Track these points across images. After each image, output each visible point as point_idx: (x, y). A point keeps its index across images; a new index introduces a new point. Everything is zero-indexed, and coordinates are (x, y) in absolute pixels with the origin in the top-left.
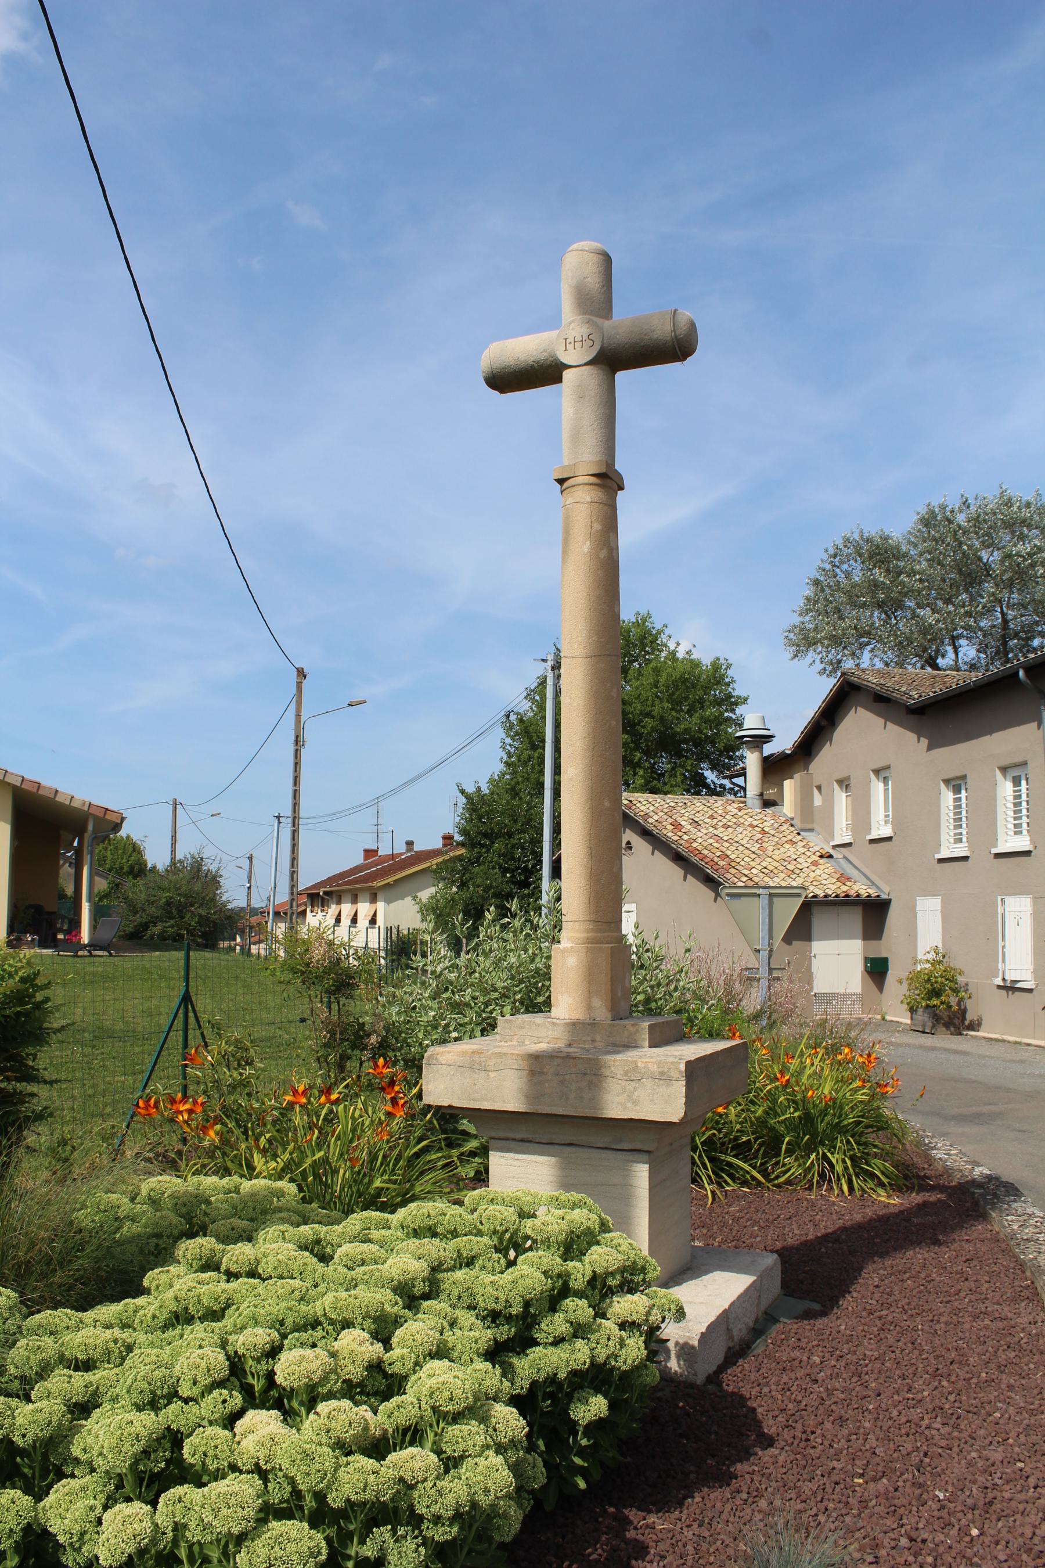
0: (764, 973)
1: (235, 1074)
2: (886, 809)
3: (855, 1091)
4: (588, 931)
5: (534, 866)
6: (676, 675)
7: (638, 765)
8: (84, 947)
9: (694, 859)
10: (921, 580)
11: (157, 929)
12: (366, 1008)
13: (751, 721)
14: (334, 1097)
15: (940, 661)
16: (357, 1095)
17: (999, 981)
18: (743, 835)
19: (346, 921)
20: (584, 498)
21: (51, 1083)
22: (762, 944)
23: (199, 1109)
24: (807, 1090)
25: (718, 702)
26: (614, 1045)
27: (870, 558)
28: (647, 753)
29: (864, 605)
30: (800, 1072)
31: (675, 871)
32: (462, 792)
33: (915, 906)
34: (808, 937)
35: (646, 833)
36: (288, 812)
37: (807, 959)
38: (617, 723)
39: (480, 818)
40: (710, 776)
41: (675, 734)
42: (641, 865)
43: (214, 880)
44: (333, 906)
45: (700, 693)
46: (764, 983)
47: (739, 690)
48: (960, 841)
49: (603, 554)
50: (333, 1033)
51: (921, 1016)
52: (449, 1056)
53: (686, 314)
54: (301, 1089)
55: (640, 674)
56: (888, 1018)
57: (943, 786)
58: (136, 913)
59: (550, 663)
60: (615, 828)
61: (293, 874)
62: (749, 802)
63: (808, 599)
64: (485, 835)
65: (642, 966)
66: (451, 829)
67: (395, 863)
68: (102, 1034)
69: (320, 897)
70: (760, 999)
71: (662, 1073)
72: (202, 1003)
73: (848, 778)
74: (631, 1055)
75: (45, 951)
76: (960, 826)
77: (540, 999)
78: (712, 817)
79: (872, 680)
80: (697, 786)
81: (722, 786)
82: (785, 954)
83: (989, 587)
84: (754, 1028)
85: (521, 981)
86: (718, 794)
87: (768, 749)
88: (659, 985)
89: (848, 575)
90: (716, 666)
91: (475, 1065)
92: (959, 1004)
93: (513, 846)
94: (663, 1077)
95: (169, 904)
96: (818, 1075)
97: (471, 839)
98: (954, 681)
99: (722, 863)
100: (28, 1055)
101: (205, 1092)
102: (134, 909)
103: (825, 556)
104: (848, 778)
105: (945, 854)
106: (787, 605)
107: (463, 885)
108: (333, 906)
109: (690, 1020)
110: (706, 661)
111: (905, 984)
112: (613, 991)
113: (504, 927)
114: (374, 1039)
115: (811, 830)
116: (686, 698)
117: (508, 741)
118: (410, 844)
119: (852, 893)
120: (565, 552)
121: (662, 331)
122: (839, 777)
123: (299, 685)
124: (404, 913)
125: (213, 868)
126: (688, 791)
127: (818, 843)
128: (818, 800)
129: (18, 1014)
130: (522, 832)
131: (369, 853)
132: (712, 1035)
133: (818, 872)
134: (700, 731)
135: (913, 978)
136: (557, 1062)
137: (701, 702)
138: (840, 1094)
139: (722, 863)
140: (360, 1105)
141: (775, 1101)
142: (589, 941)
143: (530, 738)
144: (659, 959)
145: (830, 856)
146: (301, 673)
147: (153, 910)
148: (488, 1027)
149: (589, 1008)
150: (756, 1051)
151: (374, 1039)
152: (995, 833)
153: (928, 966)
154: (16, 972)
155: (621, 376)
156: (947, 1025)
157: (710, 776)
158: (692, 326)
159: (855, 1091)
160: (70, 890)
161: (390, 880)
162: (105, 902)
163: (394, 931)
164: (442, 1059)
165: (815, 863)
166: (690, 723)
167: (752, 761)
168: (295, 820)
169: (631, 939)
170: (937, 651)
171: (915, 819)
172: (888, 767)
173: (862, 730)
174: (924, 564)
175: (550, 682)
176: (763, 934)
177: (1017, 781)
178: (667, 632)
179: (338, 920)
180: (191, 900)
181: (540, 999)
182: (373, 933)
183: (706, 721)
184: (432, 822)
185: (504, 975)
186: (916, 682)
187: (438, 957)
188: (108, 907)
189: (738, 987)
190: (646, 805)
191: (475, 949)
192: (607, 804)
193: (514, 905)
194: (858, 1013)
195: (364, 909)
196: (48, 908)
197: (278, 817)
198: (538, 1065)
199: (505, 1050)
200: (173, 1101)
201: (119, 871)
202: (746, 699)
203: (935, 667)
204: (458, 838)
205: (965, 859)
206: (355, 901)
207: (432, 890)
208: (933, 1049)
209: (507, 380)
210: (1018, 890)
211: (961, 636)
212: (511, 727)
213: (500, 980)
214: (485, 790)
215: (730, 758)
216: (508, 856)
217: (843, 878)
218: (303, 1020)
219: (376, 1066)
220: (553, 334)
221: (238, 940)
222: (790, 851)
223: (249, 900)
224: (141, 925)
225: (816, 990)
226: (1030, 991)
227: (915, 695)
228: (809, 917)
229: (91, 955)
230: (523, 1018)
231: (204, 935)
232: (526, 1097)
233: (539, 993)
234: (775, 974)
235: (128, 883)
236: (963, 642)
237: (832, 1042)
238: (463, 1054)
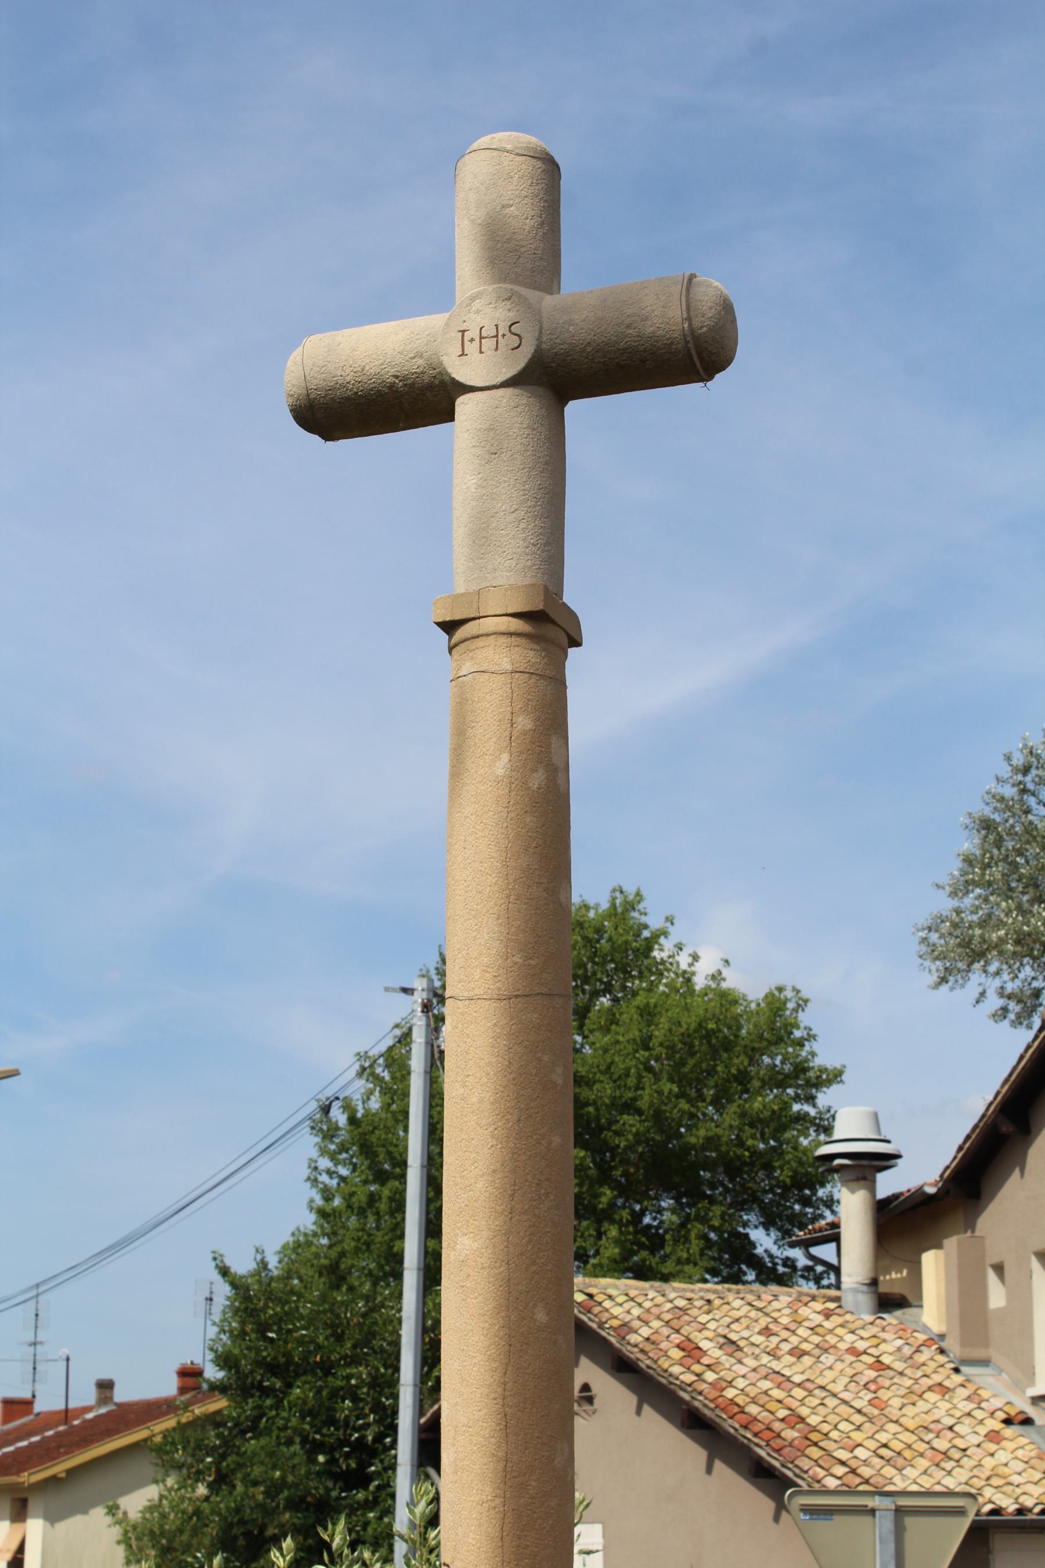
5: (379, 1438)
6: (689, 1022)
7: (606, 1215)
9: (731, 1425)
18: (835, 1372)
20: (497, 661)
25: (778, 1080)
28: (627, 1191)
31: (687, 1452)
32: (224, 1272)
35: (623, 1367)
39: (262, 1330)
40: (764, 1241)
41: (687, 1148)
42: (616, 1441)
45: (740, 1061)
47: (824, 1055)
49: (538, 779)
53: (714, 283)
59: (419, 997)
60: (559, 1359)
62: (848, 1299)
63: (969, 861)
64: (273, 1368)
67: (72, 1432)
80: (734, 1262)
86: (782, 1281)
93: (334, 1394)
97: (241, 1376)
99: (790, 1434)
106: (926, 874)
107: (221, 1481)
110: (750, 985)
115: (985, 1362)
116: (711, 1072)
117: (325, 1163)
118: (105, 1387)
121: (664, 318)
126: (714, 1272)
127: (1000, 1392)
128: (997, 1296)
130: (354, 1361)
133: (1002, 1456)
137: (743, 1078)
139: (790, 1434)
143: (374, 1154)
145: (1027, 1421)
155: (576, 410)
157: (764, 1241)
158: (727, 309)
161: (59, 1468)
165: (994, 1436)
166: (715, 1124)
167: (852, 1209)
178: (676, 934)
183: (754, 1122)
190: (622, 1303)
192: (541, 1316)
204: (213, 1373)
207: (151, 1492)
209: (338, 414)
216: (322, 1414)
220: (436, 321)
222: (940, 1408)
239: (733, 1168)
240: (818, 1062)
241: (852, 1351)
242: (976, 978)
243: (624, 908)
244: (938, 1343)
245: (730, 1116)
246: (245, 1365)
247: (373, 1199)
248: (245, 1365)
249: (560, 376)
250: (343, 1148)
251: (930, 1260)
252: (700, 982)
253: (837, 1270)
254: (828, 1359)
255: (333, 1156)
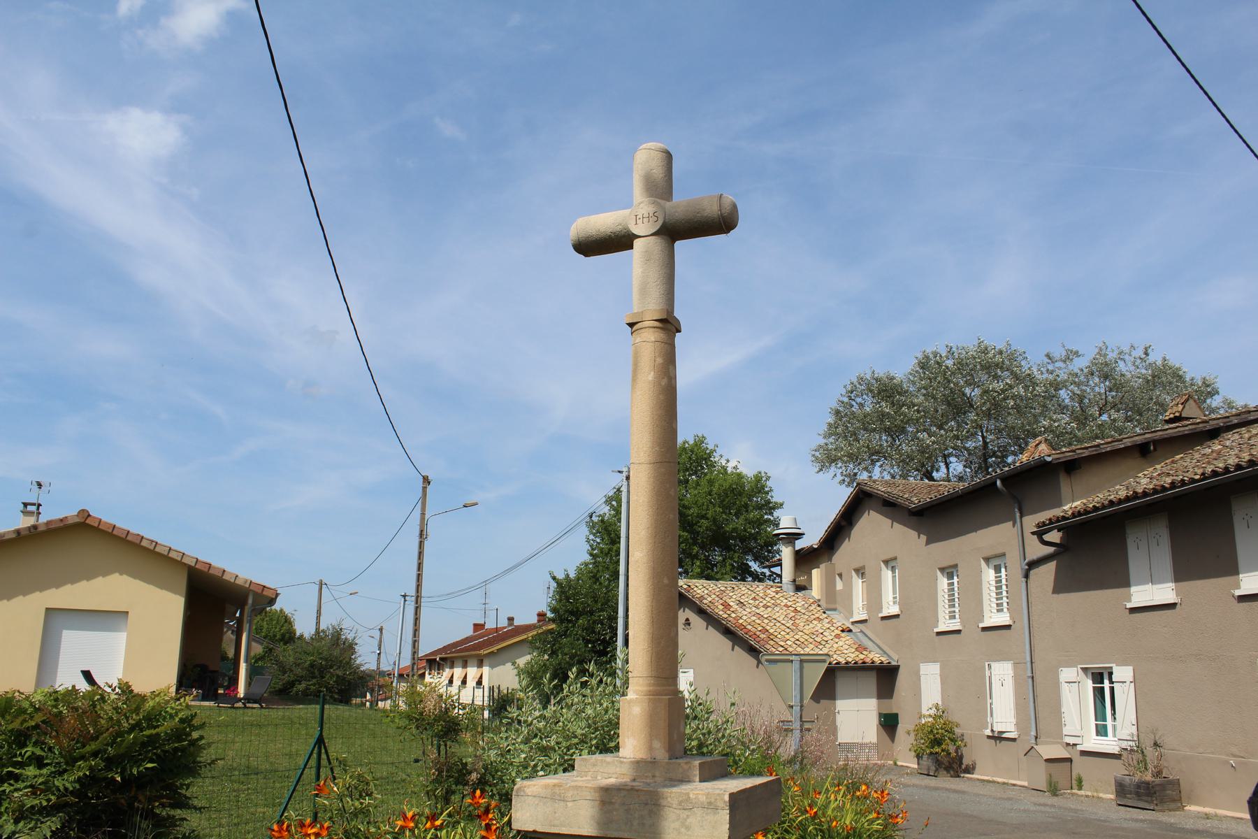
0: (797, 725)
1: (357, 803)
2: (894, 592)
3: (871, 822)
4: (649, 685)
5: (611, 638)
6: (726, 485)
7: (696, 557)
8: (240, 700)
9: (741, 633)
10: (918, 411)
11: (302, 687)
12: (468, 750)
13: (786, 522)
14: (438, 823)
15: (935, 474)
16: (459, 823)
17: (988, 732)
18: (780, 614)
19: (457, 682)
20: (649, 338)
21: (200, 809)
22: (795, 701)
23: (324, 833)
24: (831, 821)
25: (759, 507)
26: (671, 780)
27: (879, 393)
28: (703, 547)
29: (874, 430)
30: (826, 806)
31: (726, 643)
32: (554, 578)
33: (919, 671)
34: (832, 696)
35: (701, 612)
36: (412, 592)
37: (833, 714)
38: (675, 517)
39: (568, 599)
40: (754, 566)
41: (725, 532)
42: (695, 639)
43: (350, 647)
44: (447, 670)
45: (745, 499)
46: (797, 733)
47: (776, 497)
48: (954, 617)
49: (664, 382)
50: (440, 771)
51: (926, 761)
52: (534, 789)
53: (729, 197)
54: (409, 815)
55: (698, 484)
56: (899, 763)
57: (939, 573)
58: (285, 673)
59: (625, 474)
60: (673, 605)
61: (415, 643)
62: (785, 587)
63: (830, 425)
64: (572, 613)
65: (695, 718)
66: (544, 608)
67: (499, 635)
68: (250, 772)
69: (436, 662)
70: (793, 748)
71: (710, 803)
72: (336, 748)
73: (863, 567)
74: (685, 788)
75: (206, 703)
76: (954, 606)
77: (612, 744)
78: (754, 599)
79: (881, 489)
80: (743, 573)
81: (763, 574)
82: (814, 710)
83: (972, 416)
84: (788, 771)
85: (596, 729)
86: (761, 580)
87: (800, 544)
88: (709, 732)
89: (861, 405)
90: (758, 478)
91: (555, 796)
92: (956, 752)
93: (594, 622)
94: (711, 807)
95: (312, 665)
96: (840, 809)
97: (560, 616)
98: (946, 489)
99: (762, 636)
100: (182, 785)
101: (331, 818)
102: (283, 669)
103: (844, 392)
104: (863, 567)
105: (942, 628)
106: (814, 429)
107: (553, 653)
108: (447, 670)
109: (735, 762)
110: (748, 471)
111: (913, 735)
112: (670, 734)
113: (584, 685)
114: (474, 776)
115: (835, 610)
116: (734, 504)
117: (591, 537)
118: (511, 619)
119: (868, 660)
120: (634, 379)
121: (711, 210)
122: (857, 566)
123: (424, 489)
124: (505, 676)
125: (350, 637)
126: (735, 578)
127: (840, 620)
128: (839, 585)
129: (176, 750)
130: (602, 610)
131: (477, 627)
132: (753, 774)
133: (841, 643)
134: (745, 530)
135: (920, 729)
136: (623, 793)
137: (746, 506)
138: (859, 825)
139: (762, 636)
140: (460, 831)
141: (805, 830)
142: (650, 693)
143: (608, 534)
144: (709, 713)
145: (850, 631)
146: (426, 480)
147: (298, 671)
148: (569, 767)
149: (651, 748)
150: (789, 788)
151: (474, 776)
152: (982, 611)
153: (930, 719)
154: (176, 714)
155: (680, 245)
156: (948, 769)
157: (754, 566)
158: (735, 207)
159: (871, 822)
160: (231, 654)
161: (495, 649)
162: (260, 663)
163: (496, 690)
164: (528, 791)
165: (837, 636)
166: (737, 523)
167: (786, 554)
168: (418, 598)
169: (686, 695)
170: (933, 467)
171: (917, 601)
172: (895, 559)
173: (874, 529)
174: (922, 398)
175: (624, 489)
176: (795, 693)
177: (997, 569)
178: (719, 452)
179: (451, 681)
180: (331, 662)
181: (612, 744)
182: (479, 692)
183: (750, 522)
184: (529, 602)
185: (583, 724)
186: (916, 491)
187: (532, 712)
188: (262, 668)
189: (776, 737)
190: (701, 589)
191: (559, 702)
192: (666, 581)
193: (592, 667)
194: (875, 760)
195: (472, 672)
196: (212, 668)
197: (404, 596)
198: (608, 796)
199: (580, 784)
200: (302, 825)
201: (273, 639)
202: (782, 505)
203: (931, 479)
204: (550, 615)
205: (958, 632)
206: (465, 666)
207: (528, 657)
208: (936, 789)
209: (590, 247)
210: (1002, 658)
211: (950, 455)
212: (593, 527)
213: (579, 728)
214: (572, 575)
215: (769, 552)
216: (590, 629)
217: (861, 648)
218: (417, 761)
219: (474, 797)
220: (627, 212)
221: (368, 696)
222: (818, 627)
223: (378, 664)
224: (288, 682)
225: (840, 741)
226: (1014, 740)
227: (915, 501)
228: (833, 680)
229: (245, 707)
230: (598, 757)
231: (341, 692)
232: (598, 824)
233: (611, 740)
234: (807, 726)
235: (280, 648)
236: (953, 459)
237: (852, 782)
238: (546, 787)
239: (743, 540)
240: (773, 500)
241: (786, 606)
242: (833, 468)
243: (700, 441)
244: (818, 603)
245: (741, 520)
246: (561, 612)
247: (610, 550)
248: (561, 612)
249: (673, 231)
250: (598, 532)
251: (815, 572)
252: (729, 470)
253: (780, 576)
254: (777, 609)
255: (594, 535)
